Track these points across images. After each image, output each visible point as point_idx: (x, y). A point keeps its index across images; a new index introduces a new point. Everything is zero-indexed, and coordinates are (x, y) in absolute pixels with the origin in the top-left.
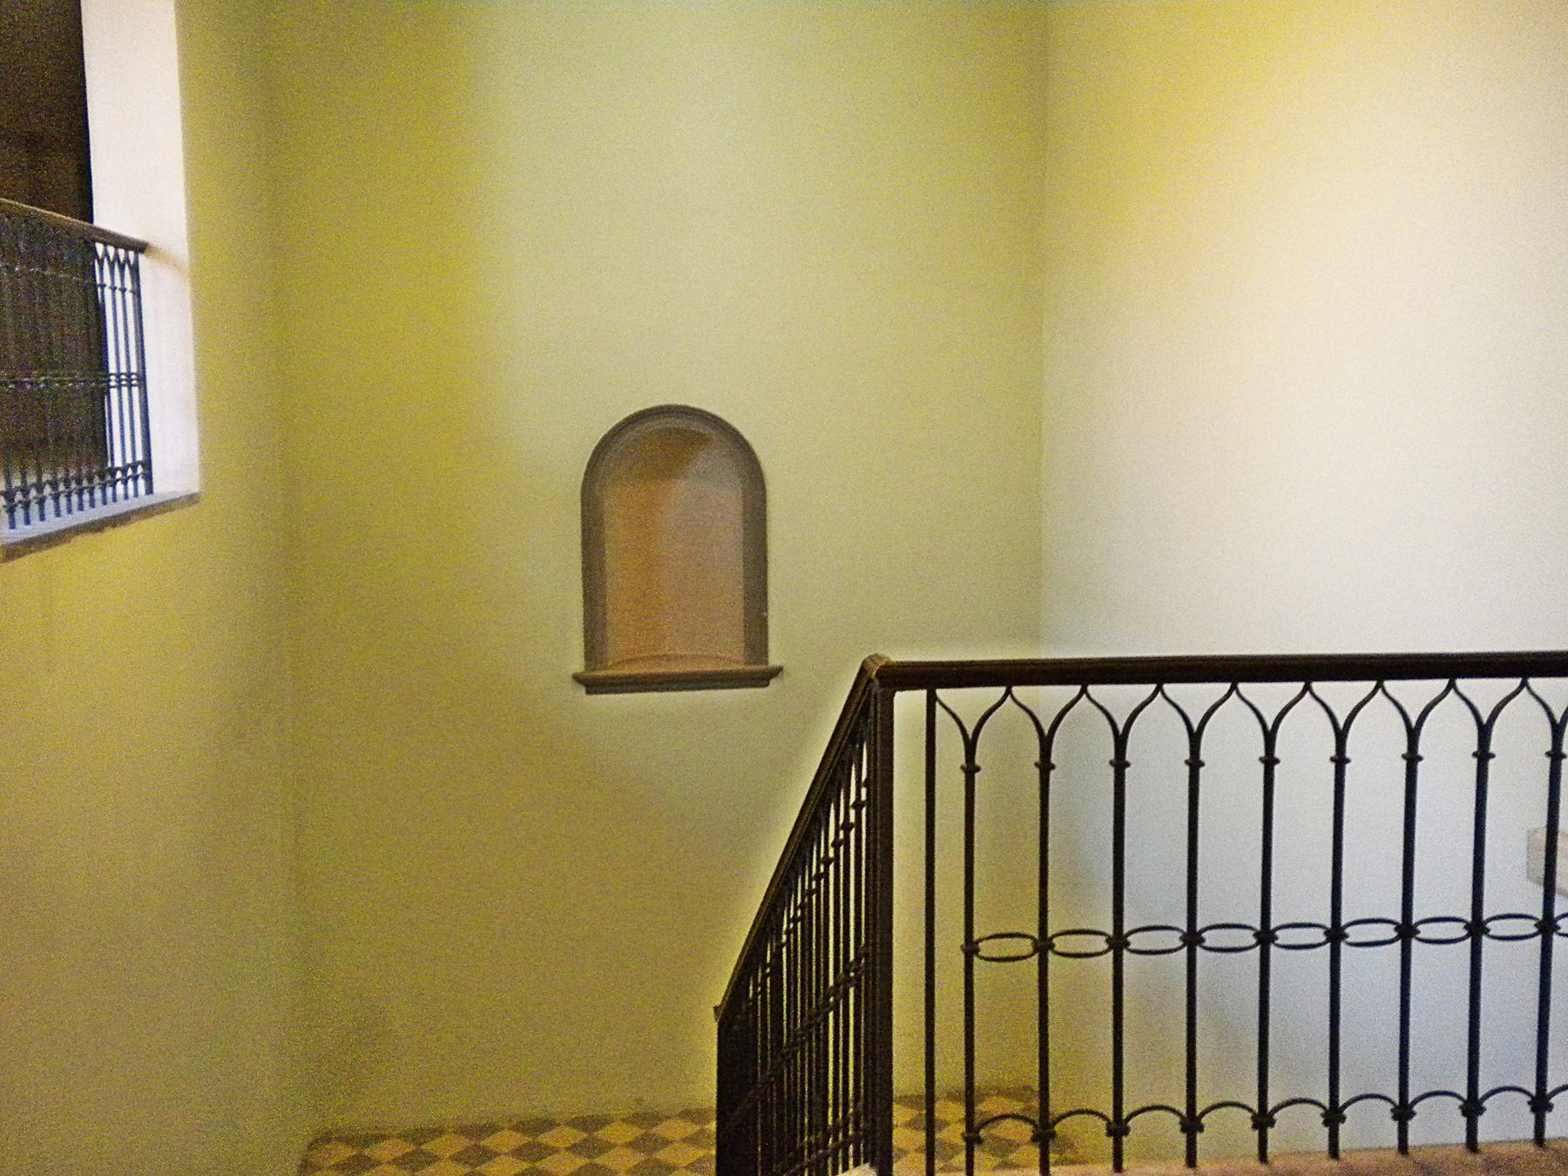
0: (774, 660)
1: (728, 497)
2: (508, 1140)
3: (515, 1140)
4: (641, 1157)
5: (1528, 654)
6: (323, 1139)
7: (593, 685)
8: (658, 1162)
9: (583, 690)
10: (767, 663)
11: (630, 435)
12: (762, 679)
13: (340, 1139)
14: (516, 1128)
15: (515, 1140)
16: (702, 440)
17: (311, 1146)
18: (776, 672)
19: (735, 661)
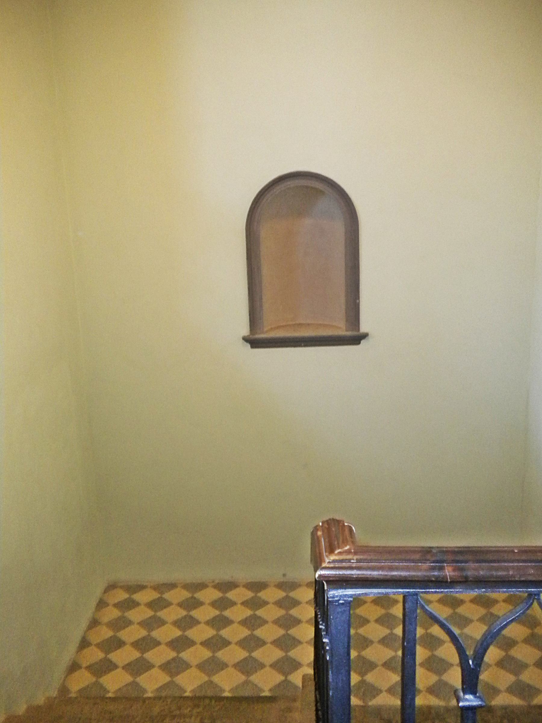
0: (364, 328)
1: (338, 228)
2: (210, 595)
3: (214, 594)
4: (282, 612)
5: (287, 346)
6: (111, 587)
7: (254, 343)
8: (291, 616)
9: (249, 345)
10: (359, 330)
11: (277, 189)
12: (357, 339)
13: (121, 587)
14: (215, 587)
15: (214, 594)
16: (322, 193)
17: (106, 591)
18: (365, 336)
19: (342, 331)
